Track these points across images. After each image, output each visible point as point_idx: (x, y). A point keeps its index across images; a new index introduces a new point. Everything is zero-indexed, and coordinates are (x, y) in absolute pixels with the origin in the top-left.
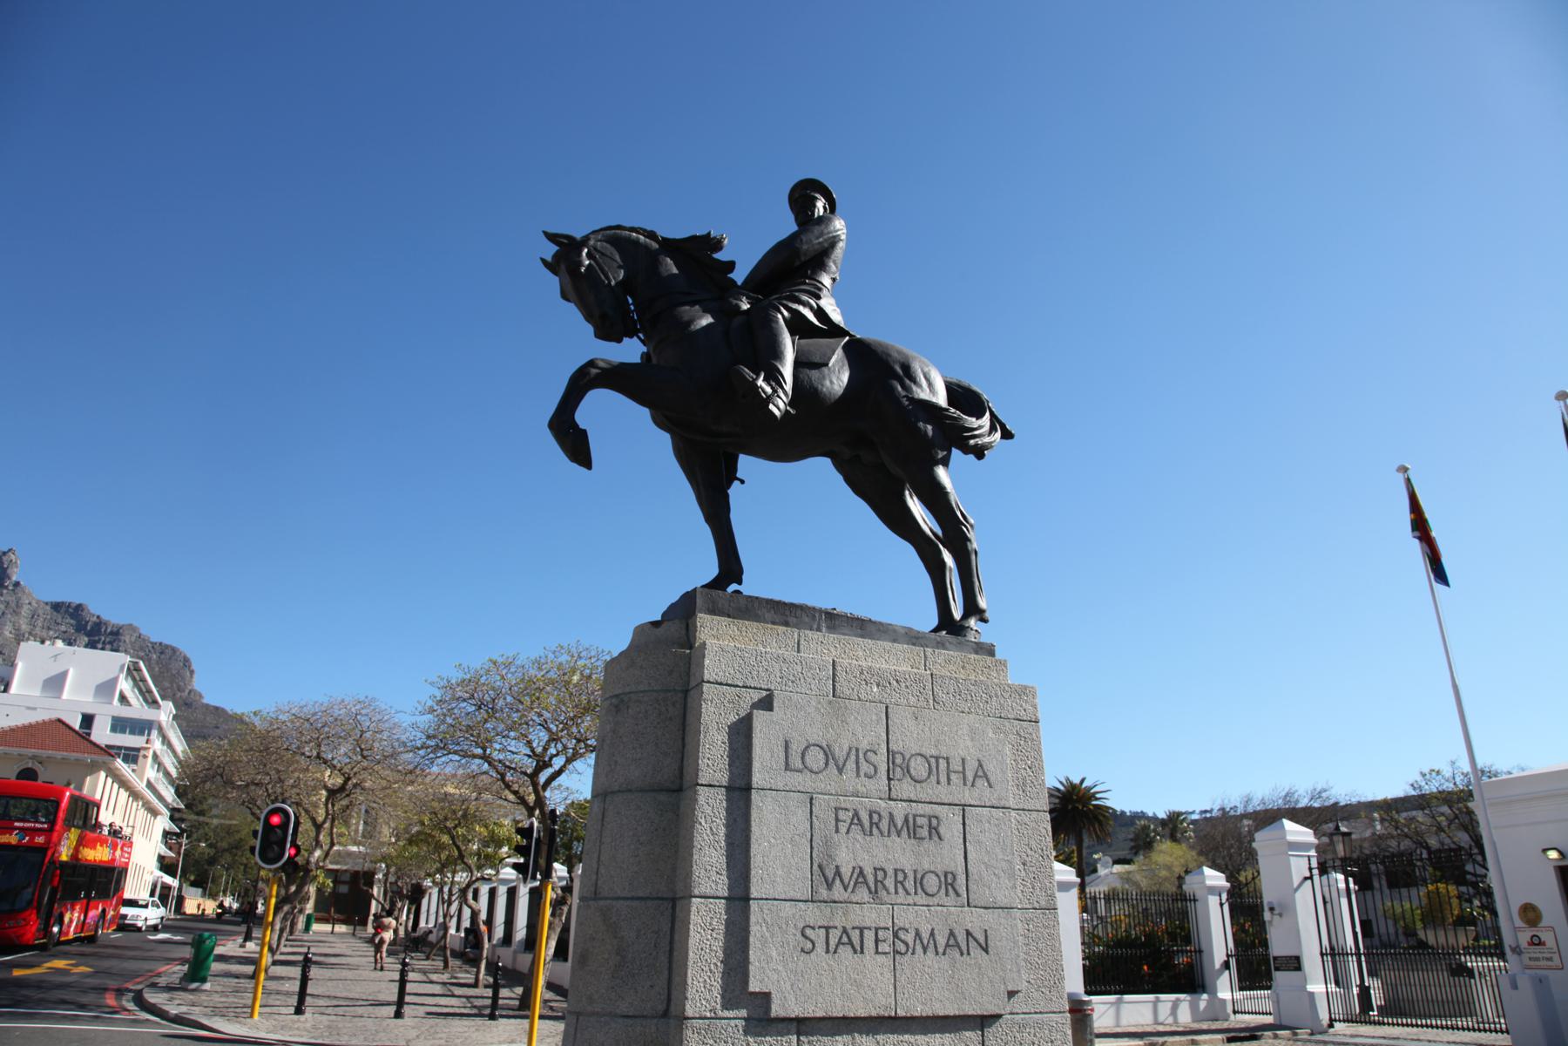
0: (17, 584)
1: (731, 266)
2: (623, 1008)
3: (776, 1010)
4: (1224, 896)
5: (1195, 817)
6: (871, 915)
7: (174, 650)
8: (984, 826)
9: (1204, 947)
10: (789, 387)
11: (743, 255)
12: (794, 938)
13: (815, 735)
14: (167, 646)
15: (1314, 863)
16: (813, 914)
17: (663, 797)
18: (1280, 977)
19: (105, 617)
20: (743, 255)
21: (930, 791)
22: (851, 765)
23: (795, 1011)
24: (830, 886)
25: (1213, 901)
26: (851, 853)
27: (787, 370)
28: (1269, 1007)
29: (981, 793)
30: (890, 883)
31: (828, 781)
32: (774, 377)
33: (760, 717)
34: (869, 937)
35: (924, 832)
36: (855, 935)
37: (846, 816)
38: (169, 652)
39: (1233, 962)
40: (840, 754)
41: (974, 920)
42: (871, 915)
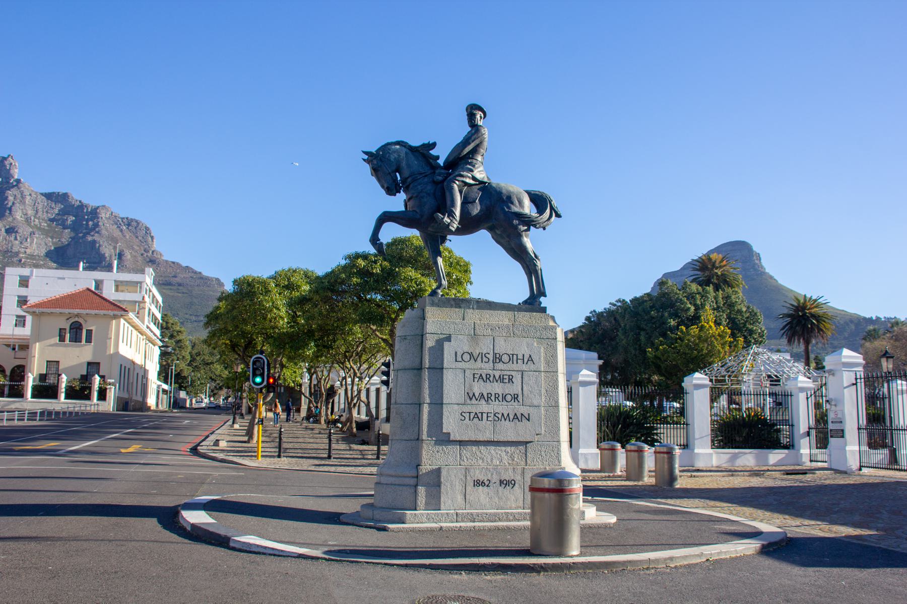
0: (18, 181)
1: (438, 158)
2: (405, 438)
3: (452, 438)
6: (484, 407)
7: (138, 222)
8: (530, 379)
9: (795, 423)
10: (458, 218)
11: (442, 153)
12: (458, 416)
13: (466, 349)
14: (132, 220)
17: (415, 371)
18: (833, 441)
19: (85, 202)
20: (442, 153)
21: (510, 366)
22: (479, 358)
23: (458, 439)
24: (471, 399)
25: (802, 396)
26: (478, 388)
27: (458, 212)
28: (826, 458)
30: (493, 398)
31: (471, 365)
32: (451, 215)
33: (446, 344)
34: (485, 415)
35: (507, 381)
36: (480, 415)
38: (134, 224)
39: (813, 432)
40: (475, 355)
41: (524, 410)
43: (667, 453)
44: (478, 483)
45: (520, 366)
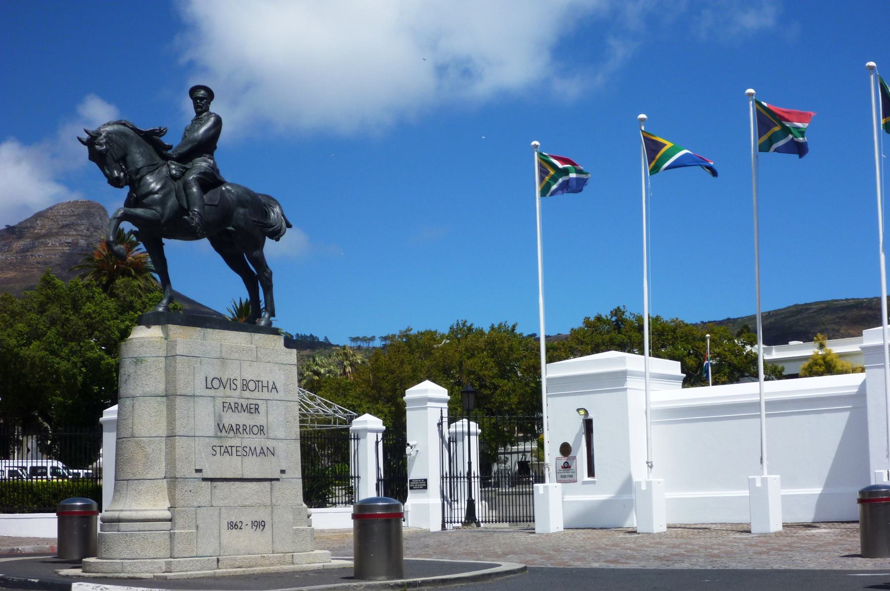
4: (380, 436)
5: (378, 343)
6: (236, 442)
15: (445, 414)
16: (216, 442)
21: (256, 394)
22: (228, 386)
26: (232, 418)
29: (273, 395)
30: (241, 430)
31: (221, 392)
34: (234, 449)
35: (253, 411)
37: (226, 405)
40: (224, 381)
41: (270, 444)
42: (236, 442)
43: (170, 520)
44: (233, 526)
45: (265, 395)
